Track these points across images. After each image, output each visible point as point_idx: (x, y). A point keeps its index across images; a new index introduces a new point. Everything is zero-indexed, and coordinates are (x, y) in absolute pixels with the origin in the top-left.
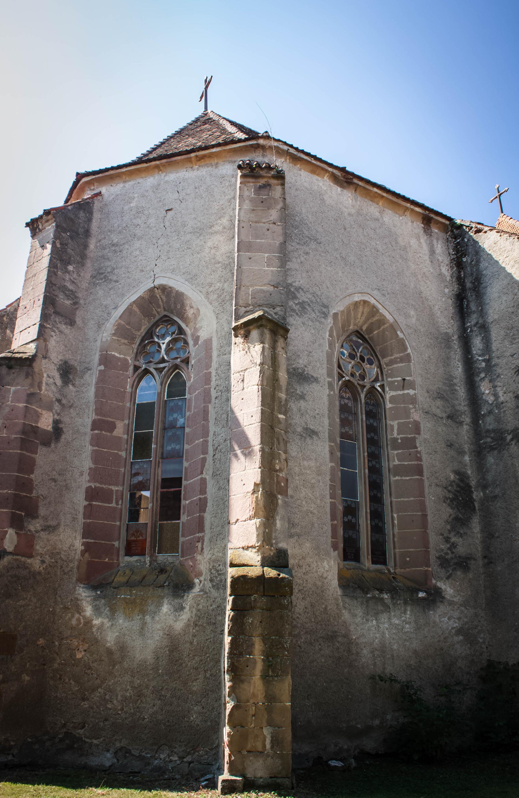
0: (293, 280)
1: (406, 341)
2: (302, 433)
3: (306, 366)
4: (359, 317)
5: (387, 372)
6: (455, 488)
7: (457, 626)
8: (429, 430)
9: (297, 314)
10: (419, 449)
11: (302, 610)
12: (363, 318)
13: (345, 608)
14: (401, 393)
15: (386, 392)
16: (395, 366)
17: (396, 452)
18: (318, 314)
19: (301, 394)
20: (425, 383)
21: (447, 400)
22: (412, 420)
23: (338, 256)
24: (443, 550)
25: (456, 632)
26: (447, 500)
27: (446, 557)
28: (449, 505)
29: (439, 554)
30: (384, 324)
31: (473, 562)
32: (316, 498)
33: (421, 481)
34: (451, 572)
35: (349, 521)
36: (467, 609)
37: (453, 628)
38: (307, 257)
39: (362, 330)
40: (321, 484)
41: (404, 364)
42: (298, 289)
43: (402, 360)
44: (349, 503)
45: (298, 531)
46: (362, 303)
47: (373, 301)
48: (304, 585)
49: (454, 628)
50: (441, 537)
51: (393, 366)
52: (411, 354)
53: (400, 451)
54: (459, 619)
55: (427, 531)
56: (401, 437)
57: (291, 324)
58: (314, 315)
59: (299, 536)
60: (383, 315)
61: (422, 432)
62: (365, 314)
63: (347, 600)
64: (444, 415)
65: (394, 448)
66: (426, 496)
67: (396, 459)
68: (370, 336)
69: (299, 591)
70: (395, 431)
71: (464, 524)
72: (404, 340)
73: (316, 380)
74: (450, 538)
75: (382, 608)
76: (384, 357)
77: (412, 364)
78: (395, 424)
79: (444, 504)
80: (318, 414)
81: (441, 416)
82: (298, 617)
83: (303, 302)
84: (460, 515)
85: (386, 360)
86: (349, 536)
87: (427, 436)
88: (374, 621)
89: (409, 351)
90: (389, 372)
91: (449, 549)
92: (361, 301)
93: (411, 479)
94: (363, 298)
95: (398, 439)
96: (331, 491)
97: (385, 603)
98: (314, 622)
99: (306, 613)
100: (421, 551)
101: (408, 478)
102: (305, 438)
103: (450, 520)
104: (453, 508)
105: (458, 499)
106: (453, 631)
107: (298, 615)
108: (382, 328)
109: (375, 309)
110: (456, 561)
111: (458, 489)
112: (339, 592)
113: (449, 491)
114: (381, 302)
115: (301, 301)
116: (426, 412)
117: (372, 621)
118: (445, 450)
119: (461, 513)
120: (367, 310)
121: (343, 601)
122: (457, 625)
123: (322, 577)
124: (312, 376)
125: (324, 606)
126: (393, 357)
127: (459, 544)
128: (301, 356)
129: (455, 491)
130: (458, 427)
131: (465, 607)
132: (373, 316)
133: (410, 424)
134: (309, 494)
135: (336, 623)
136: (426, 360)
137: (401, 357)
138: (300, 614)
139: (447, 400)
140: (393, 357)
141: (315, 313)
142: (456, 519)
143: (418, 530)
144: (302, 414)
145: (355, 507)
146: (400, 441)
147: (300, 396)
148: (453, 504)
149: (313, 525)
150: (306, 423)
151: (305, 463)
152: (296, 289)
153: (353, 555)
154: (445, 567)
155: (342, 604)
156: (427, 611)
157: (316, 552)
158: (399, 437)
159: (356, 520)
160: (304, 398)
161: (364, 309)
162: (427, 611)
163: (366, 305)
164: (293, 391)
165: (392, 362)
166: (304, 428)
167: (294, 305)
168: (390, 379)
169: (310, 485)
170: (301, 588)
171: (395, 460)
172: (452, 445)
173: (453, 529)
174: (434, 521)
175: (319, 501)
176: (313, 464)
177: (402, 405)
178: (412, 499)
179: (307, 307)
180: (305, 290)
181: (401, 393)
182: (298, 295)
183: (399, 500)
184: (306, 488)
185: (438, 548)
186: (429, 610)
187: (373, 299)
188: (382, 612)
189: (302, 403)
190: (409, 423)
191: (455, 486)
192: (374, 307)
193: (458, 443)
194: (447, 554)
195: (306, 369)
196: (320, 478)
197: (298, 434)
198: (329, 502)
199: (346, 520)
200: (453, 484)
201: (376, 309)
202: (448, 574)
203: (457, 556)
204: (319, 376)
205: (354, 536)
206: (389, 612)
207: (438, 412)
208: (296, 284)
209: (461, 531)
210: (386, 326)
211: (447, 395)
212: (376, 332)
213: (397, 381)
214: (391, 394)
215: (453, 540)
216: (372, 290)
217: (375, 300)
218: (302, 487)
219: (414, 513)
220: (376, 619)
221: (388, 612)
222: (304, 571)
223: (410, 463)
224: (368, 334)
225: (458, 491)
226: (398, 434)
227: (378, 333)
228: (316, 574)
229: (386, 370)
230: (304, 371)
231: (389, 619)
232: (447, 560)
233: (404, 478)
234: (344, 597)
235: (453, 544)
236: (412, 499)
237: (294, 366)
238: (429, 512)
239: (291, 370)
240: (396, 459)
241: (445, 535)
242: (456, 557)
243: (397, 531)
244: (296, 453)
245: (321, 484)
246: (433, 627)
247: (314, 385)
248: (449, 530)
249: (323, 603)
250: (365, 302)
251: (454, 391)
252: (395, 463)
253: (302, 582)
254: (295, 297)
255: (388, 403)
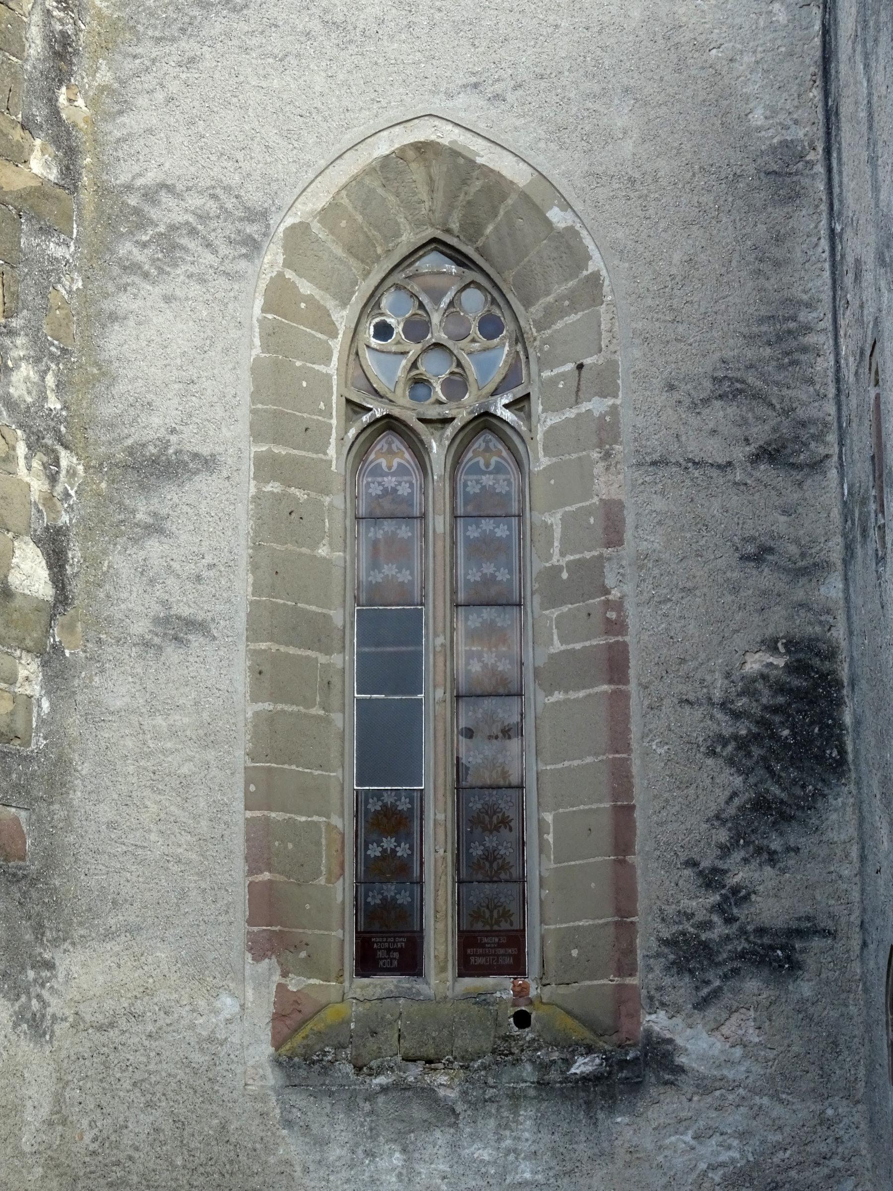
0: (136, 169)
1: (584, 233)
2: (148, 637)
3: (173, 431)
4: (425, 196)
5: (541, 350)
6: (764, 701)
7: (733, 1161)
8: (660, 523)
9: (146, 275)
10: (615, 594)
11: (143, 1136)
12: (440, 195)
13: (288, 1124)
14: (570, 414)
15: (534, 419)
16: (559, 325)
17: (555, 613)
18: (224, 250)
19: (150, 520)
20: (660, 361)
21: (757, 396)
22: (596, 500)
23: (316, 26)
24: (689, 916)
25: (724, 1177)
26: (725, 746)
27: (703, 937)
28: (731, 762)
29: (675, 929)
30: (503, 197)
31: (817, 943)
32: (196, 817)
33: (619, 700)
34: (717, 983)
35: (388, 856)
36: (781, 1101)
37: (712, 1167)
38: (192, 75)
39: (448, 231)
40: (214, 771)
41: (580, 314)
42: (150, 195)
43: (574, 302)
44: (388, 800)
45: (132, 919)
46: (411, 154)
47: (447, 135)
48: (151, 1067)
49: (722, 1165)
50: (688, 872)
51: (554, 327)
52: (604, 273)
53: (565, 609)
54: (743, 1135)
55: (630, 858)
56: (569, 563)
57: (120, 313)
58: (209, 258)
59: (133, 930)
60: (492, 171)
61: (628, 535)
62: (440, 184)
63: (298, 1099)
64: (739, 453)
65: (552, 601)
66: (634, 745)
67: (555, 637)
68: (480, 243)
69: (135, 1084)
70: (556, 544)
71: (790, 818)
72: (577, 233)
73: (209, 463)
74: (725, 872)
75: (426, 1116)
76: (527, 303)
77: (603, 308)
78: (554, 520)
79: (710, 762)
80: (211, 566)
81: (721, 460)
82: (130, 1158)
83: (173, 228)
84: (775, 790)
85: (537, 310)
86: (384, 899)
87: (654, 542)
88: (397, 1155)
89: (596, 264)
90: (546, 348)
91: (719, 908)
92: (403, 149)
93: (589, 695)
94: (412, 139)
95: (559, 569)
96: (252, 788)
97: (437, 1100)
98: (184, 1167)
99: (157, 1144)
100: (607, 924)
101: (581, 694)
102: (160, 648)
103: (732, 810)
104: (746, 773)
105: (774, 736)
106: (717, 1176)
107: (131, 1152)
108: (502, 212)
109: (461, 161)
110: (741, 945)
111: (781, 700)
112: (272, 1078)
113: (736, 715)
114: (481, 127)
115: (162, 229)
116: (654, 463)
117: (391, 1155)
118: (735, 575)
119: (778, 781)
120: (438, 169)
121: (281, 1102)
122: (737, 1155)
123: (210, 1040)
124: (196, 456)
125: (216, 1122)
126: (550, 299)
127: (761, 888)
128: (157, 403)
129: (765, 708)
130: (800, 484)
131: (775, 1097)
132: (464, 182)
133: (590, 514)
134: (173, 808)
135: (256, 1168)
136: (673, 277)
137: (573, 291)
138: (137, 1149)
139: (757, 396)
140: (550, 299)
141: (215, 252)
142: (761, 805)
143: (600, 859)
144: (152, 582)
145: (411, 810)
146: (565, 575)
147: (147, 527)
148: (749, 755)
149: (183, 894)
150: (165, 604)
151: (159, 720)
152: (145, 195)
153: (396, 955)
154: (691, 972)
155: (278, 1111)
156: (601, 1115)
157: (192, 970)
158: (563, 563)
159: (411, 848)
160: (160, 531)
161: (428, 167)
162: (601, 1115)
163: (430, 155)
164: (122, 517)
165: (551, 315)
166: (156, 621)
167: (135, 251)
168: (546, 374)
169: (174, 783)
170: (138, 1076)
171: (552, 640)
172: (770, 550)
173: (739, 838)
174: (661, 824)
175: (204, 823)
176: (186, 720)
177: (574, 456)
178: (589, 760)
179: (184, 241)
180: (180, 187)
181: (570, 414)
182: (154, 213)
183: (560, 766)
184: (160, 792)
185: (671, 910)
186: (612, 1110)
187: (450, 127)
188: (427, 1126)
189: (154, 547)
190: (588, 511)
191: (766, 692)
192: (454, 153)
193: (797, 541)
194: (707, 925)
195: (174, 438)
196: (210, 755)
197: (136, 640)
198: (242, 822)
199: (375, 851)
200: (759, 685)
201: (464, 157)
202: (705, 991)
203: (750, 928)
204: (219, 449)
205: (403, 899)
206: (454, 1125)
207: (714, 450)
208: (151, 177)
209: (776, 844)
210: (510, 201)
211: (762, 375)
212: (489, 229)
213: (563, 376)
214: (549, 423)
215: (739, 875)
216: (450, 96)
217: (457, 130)
218: (147, 792)
219: (594, 806)
220: (404, 1150)
221: (450, 1126)
222: (150, 1027)
223: (587, 644)
224: (471, 240)
225: (776, 710)
226: (562, 554)
227: (496, 229)
228: (188, 1034)
229: (537, 343)
230: (167, 445)
231: (454, 1146)
232: (705, 945)
233: (573, 695)
234: (287, 1091)
235: (735, 890)
236: (589, 760)
237: (129, 442)
238: (639, 797)
239: (121, 456)
240: (555, 637)
241: (705, 864)
242: (743, 931)
243: (553, 866)
244: (127, 699)
245: (214, 771)
246: (628, 1165)
247: (203, 483)
248: (721, 847)
249: (214, 1115)
250: (422, 148)
251: (796, 356)
252: (552, 650)
253: (144, 1059)
254: (141, 221)
255: (541, 453)
